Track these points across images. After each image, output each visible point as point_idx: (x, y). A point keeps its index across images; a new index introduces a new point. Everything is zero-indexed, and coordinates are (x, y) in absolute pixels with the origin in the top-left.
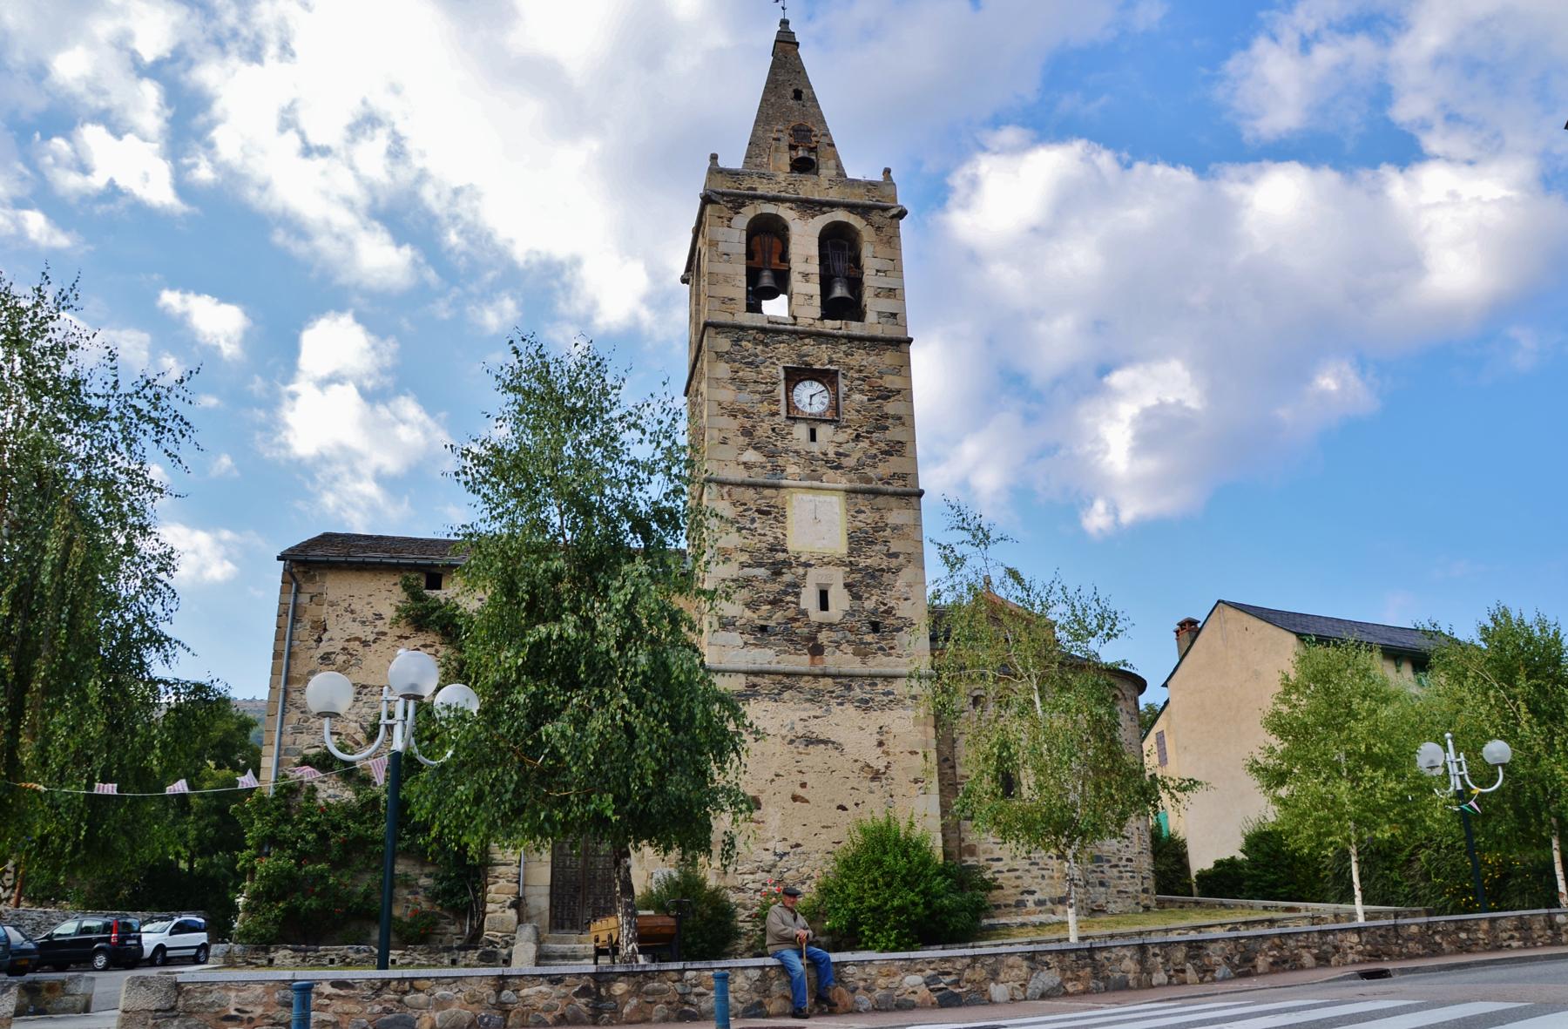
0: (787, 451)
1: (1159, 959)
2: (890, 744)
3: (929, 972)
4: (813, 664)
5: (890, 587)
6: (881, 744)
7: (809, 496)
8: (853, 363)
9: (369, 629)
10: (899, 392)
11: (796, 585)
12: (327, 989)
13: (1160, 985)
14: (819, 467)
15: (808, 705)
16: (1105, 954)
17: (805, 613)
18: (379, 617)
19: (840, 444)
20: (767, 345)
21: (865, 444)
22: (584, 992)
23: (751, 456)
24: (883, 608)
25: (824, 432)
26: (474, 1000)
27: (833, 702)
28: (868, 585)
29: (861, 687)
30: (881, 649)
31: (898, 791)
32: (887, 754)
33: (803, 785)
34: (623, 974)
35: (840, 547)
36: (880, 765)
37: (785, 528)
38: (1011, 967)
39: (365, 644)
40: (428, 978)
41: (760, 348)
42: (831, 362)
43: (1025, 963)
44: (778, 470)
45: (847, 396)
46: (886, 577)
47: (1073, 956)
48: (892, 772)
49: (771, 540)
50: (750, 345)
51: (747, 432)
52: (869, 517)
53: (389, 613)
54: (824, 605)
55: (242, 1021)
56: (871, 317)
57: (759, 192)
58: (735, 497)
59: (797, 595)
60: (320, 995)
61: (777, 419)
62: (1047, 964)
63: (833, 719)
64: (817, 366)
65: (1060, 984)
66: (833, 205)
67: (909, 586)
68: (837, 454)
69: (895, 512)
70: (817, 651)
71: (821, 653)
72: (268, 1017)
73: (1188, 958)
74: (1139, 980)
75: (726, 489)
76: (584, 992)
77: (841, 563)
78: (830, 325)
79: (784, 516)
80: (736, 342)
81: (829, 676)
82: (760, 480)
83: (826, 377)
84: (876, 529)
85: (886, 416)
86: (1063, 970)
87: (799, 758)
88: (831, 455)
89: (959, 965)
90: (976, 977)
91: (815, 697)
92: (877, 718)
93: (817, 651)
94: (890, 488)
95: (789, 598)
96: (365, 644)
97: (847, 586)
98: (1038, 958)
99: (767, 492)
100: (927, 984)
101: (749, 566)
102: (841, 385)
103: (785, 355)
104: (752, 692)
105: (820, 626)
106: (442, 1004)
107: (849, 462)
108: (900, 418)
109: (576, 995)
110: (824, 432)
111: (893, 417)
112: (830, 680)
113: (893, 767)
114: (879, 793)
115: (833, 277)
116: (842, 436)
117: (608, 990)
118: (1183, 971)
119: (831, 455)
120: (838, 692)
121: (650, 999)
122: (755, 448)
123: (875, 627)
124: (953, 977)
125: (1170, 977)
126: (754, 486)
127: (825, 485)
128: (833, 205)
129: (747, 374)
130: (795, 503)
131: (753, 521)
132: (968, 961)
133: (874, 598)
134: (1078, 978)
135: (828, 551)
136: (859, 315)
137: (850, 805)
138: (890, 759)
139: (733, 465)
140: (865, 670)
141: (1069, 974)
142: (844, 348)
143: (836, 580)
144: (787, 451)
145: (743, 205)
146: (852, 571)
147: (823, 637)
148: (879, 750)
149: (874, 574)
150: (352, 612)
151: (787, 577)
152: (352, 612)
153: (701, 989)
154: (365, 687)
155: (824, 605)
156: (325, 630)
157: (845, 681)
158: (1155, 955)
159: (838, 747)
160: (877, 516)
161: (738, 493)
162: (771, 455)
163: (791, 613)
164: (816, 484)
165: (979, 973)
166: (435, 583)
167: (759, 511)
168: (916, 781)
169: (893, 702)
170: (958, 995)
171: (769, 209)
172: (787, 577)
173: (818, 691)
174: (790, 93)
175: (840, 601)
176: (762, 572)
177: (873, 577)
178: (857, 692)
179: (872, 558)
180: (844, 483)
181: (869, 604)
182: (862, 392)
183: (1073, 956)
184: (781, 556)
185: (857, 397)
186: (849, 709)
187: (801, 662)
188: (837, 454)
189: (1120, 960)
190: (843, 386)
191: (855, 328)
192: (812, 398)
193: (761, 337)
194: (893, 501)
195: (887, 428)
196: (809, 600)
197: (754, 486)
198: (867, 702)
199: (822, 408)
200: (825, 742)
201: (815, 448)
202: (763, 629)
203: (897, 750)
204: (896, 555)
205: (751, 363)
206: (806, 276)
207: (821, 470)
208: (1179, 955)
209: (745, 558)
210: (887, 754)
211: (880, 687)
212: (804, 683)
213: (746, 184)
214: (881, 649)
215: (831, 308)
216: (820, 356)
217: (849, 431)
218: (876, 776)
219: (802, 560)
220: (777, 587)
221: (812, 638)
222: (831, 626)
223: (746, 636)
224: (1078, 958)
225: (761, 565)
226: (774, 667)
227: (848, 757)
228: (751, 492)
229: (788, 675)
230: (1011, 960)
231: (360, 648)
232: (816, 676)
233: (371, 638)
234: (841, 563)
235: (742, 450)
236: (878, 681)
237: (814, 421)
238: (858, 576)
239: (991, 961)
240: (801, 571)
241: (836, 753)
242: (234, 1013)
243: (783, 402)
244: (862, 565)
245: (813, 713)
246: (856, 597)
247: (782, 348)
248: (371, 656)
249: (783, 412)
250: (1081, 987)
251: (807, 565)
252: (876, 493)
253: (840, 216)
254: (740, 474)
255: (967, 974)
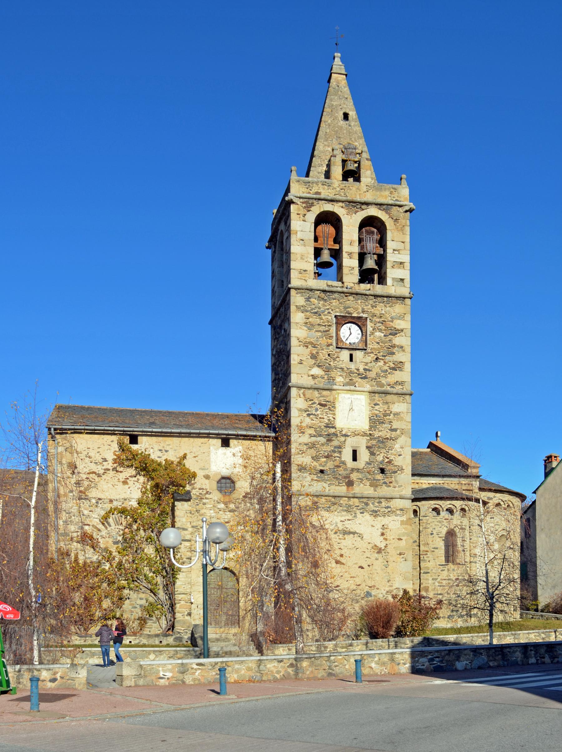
0: (336, 368)
1: (533, 652)
2: (388, 535)
3: (430, 657)
4: (348, 490)
5: (391, 448)
6: (383, 534)
7: (348, 395)
8: (377, 313)
9: (100, 467)
10: (402, 330)
11: (340, 447)
12: (195, 666)
13: (532, 664)
14: (353, 379)
15: (345, 513)
16: (508, 650)
17: (344, 463)
18: (105, 460)
19: (366, 364)
20: (325, 301)
21: (381, 363)
22: (292, 665)
23: (316, 371)
24: (387, 460)
25: (358, 355)
26: (249, 669)
27: (358, 512)
28: (379, 447)
29: (373, 504)
30: (385, 483)
31: (391, 559)
32: (386, 539)
33: (342, 556)
34: (306, 658)
35: (365, 425)
36: (382, 546)
37: (334, 414)
38: (465, 655)
39: (99, 476)
40: (232, 661)
41: (322, 302)
42: (363, 312)
43: (472, 653)
44: (332, 380)
45: (372, 333)
46: (389, 443)
47: (493, 651)
48: (388, 550)
49: (327, 421)
50: (316, 301)
51: (314, 357)
52: (381, 408)
53: (110, 457)
54: (355, 459)
55: (165, 678)
56: (389, 281)
57: (322, 196)
58: (307, 396)
59: (340, 452)
60: (192, 668)
61: (331, 347)
62: (481, 654)
63: (358, 521)
64: (355, 315)
65: (487, 662)
66: (367, 204)
67: (402, 448)
68: (365, 369)
69: (397, 404)
70: (350, 484)
71: (353, 485)
72: (174, 677)
73: (546, 651)
74: (522, 661)
75: (302, 391)
76: (292, 665)
77: (365, 434)
78: (364, 287)
79: (334, 407)
80: (308, 299)
81: (357, 498)
82: (321, 386)
83: (360, 322)
84: (385, 415)
85: (394, 346)
86: (488, 656)
87: (339, 541)
88: (361, 370)
89: (443, 654)
90: (450, 659)
91: (349, 509)
92: (381, 521)
93: (350, 484)
94: (395, 391)
95: (336, 455)
96: (99, 476)
97: (368, 447)
98: (478, 651)
99: (325, 393)
100: (429, 662)
101: (314, 436)
102: (369, 327)
103: (336, 307)
104: (315, 507)
105: (353, 470)
106: (237, 671)
107: (372, 374)
108: (402, 347)
109: (288, 667)
110: (358, 355)
111: (398, 346)
112: (356, 500)
113: (389, 547)
114: (381, 560)
115: (365, 254)
116: (369, 359)
117: (300, 664)
118: (544, 658)
119: (361, 370)
120: (361, 507)
121: (317, 668)
122: (319, 366)
123: (382, 471)
124: (440, 659)
125: (537, 660)
126: (317, 389)
127: (357, 389)
128: (367, 204)
129: (314, 320)
130: (340, 399)
131: (317, 410)
132: (447, 652)
133: (382, 455)
134: (495, 660)
135: (358, 428)
136: (382, 280)
137: (365, 566)
138: (388, 542)
139: (305, 377)
140: (376, 494)
141: (491, 658)
142: (371, 302)
143: (362, 444)
144: (336, 368)
145: (312, 205)
146: (371, 439)
147: (354, 476)
148: (382, 538)
149: (383, 441)
150: (90, 457)
151: (335, 443)
152: (90, 457)
153: (336, 664)
154: (100, 499)
155: (355, 459)
156: (76, 467)
157: (365, 500)
158: (531, 650)
159: (361, 536)
160: (386, 407)
161: (309, 393)
162: (328, 370)
163: (337, 463)
164: (352, 388)
165: (452, 657)
166: (134, 440)
167: (320, 404)
168: (400, 554)
169: (390, 512)
170: (442, 666)
171: (328, 207)
172: (335, 443)
173: (350, 506)
174: (341, 116)
175: (364, 456)
176: (322, 440)
177: (383, 442)
178: (371, 507)
179: (383, 432)
180: (368, 388)
181: (380, 458)
182: (380, 330)
183: (493, 651)
184: (333, 430)
185: (378, 334)
186: (367, 516)
187: (342, 489)
188: (365, 369)
189: (514, 652)
190: (370, 326)
191: (378, 289)
192: (351, 334)
193: (323, 295)
194: (395, 397)
195: (394, 353)
196: (347, 455)
197: (317, 389)
198: (376, 512)
199: (357, 341)
200: (354, 533)
201: (352, 366)
202: (322, 471)
203: (392, 538)
204: (395, 430)
205: (316, 313)
206: (350, 254)
207: (355, 379)
208: (543, 651)
209: (312, 431)
210: (386, 539)
211: (384, 504)
212: (344, 501)
213: (315, 189)
214: (385, 483)
215: (366, 276)
216: (357, 307)
217: (372, 355)
218: (380, 551)
219: (344, 433)
220: (329, 448)
221: (347, 477)
222: (358, 470)
223: (312, 476)
224: (496, 651)
225: (320, 436)
226: (327, 492)
227: (365, 541)
228: (316, 393)
229: (335, 497)
230: (466, 652)
231: (96, 478)
232: (349, 498)
233: (102, 472)
234: (365, 434)
235: (311, 367)
236: (382, 500)
237: (352, 349)
238: (374, 442)
239: (457, 652)
240: (343, 439)
241: (359, 539)
242: (163, 676)
243: (334, 338)
244: (376, 436)
245: (347, 518)
246: (372, 454)
247: (335, 303)
248: (102, 482)
249: (334, 344)
250: (496, 664)
251: (346, 435)
252: (386, 393)
253: (373, 211)
254: (310, 382)
255: (447, 658)
